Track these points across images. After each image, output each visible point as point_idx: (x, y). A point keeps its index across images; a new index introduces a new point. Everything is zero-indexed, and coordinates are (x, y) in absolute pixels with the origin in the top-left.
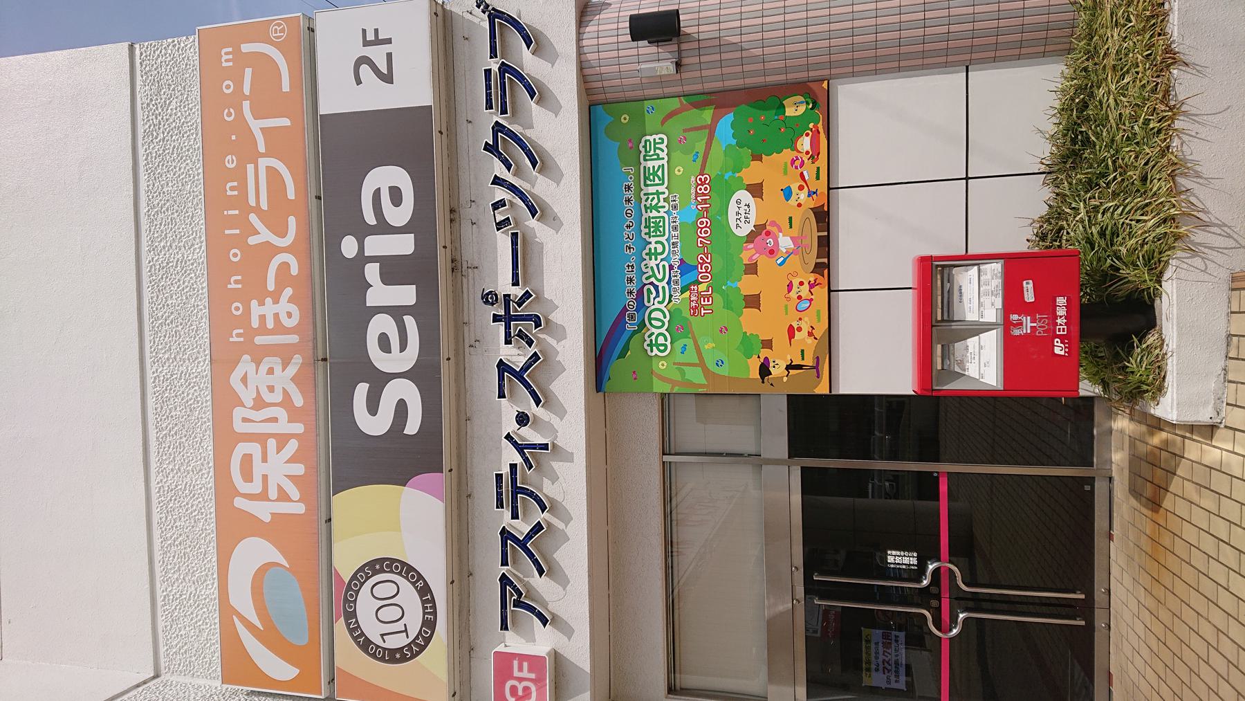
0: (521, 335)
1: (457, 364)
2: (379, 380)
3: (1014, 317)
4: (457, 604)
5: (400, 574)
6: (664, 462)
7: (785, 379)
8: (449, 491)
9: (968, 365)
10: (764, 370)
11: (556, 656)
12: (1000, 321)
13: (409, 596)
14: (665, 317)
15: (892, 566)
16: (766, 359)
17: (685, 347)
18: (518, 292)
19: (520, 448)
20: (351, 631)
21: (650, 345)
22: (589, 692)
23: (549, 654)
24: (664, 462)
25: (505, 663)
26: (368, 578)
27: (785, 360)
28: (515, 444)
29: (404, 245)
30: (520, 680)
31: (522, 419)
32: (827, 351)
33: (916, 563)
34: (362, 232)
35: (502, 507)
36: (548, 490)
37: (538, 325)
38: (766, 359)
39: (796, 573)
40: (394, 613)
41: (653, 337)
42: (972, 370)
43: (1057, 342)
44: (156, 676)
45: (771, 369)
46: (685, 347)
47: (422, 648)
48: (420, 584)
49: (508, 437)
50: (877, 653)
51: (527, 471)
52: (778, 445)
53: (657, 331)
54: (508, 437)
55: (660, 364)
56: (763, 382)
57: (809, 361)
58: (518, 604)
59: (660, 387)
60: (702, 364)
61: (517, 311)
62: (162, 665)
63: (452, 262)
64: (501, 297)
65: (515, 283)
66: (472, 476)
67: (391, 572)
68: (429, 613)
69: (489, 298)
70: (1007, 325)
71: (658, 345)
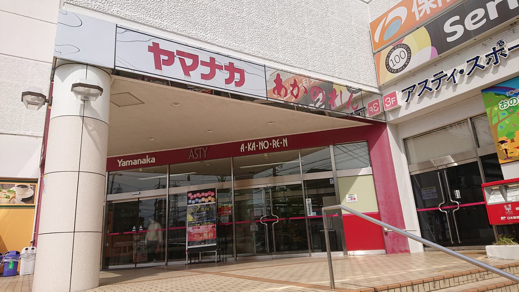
0: (490, 59)
1: (475, 43)
2: (461, 22)
3: (510, 205)
4: (405, 76)
5: (408, 57)
6: (467, 119)
7: (501, 149)
8: (436, 58)
9: (493, 196)
10: (503, 142)
11: (400, 107)
12: (508, 202)
13: (403, 62)
14: (514, 104)
15: (455, 192)
16: (507, 142)
17: (505, 114)
18: (507, 53)
19: (452, 75)
20: (390, 51)
21: (502, 102)
22: (394, 119)
23: (399, 105)
24: (467, 119)
25: (394, 95)
26: (404, 48)
27: (508, 147)
28: (453, 72)
30: (391, 101)
31: (462, 72)
32: (515, 160)
33: (458, 198)
35: (434, 77)
36: (443, 88)
37: (495, 64)
38: (507, 142)
39: (445, 166)
40: (398, 61)
41: (506, 103)
42: (492, 197)
43: (505, 217)
44: (367, 3)
45: (504, 144)
46: (505, 114)
47: (391, 72)
48: (406, 64)
49: (455, 69)
50: (430, 191)
51: (446, 80)
52: (482, 152)
53: (508, 103)
54: (455, 69)
55: (496, 108)
56: (498, 143)
57: (509, 155)
58: (409, 92)
59: (488, 110)
60: (500, 121)
61: (498, 54)
62: (370, 3)
63: (514, 23)
64: (503, 46)
65: (509, 50)
66: (442, 63)
67: (408, 54)
68: (400, 70)
69: (501, 43)
70: (507, 204)
71: (503, 105)
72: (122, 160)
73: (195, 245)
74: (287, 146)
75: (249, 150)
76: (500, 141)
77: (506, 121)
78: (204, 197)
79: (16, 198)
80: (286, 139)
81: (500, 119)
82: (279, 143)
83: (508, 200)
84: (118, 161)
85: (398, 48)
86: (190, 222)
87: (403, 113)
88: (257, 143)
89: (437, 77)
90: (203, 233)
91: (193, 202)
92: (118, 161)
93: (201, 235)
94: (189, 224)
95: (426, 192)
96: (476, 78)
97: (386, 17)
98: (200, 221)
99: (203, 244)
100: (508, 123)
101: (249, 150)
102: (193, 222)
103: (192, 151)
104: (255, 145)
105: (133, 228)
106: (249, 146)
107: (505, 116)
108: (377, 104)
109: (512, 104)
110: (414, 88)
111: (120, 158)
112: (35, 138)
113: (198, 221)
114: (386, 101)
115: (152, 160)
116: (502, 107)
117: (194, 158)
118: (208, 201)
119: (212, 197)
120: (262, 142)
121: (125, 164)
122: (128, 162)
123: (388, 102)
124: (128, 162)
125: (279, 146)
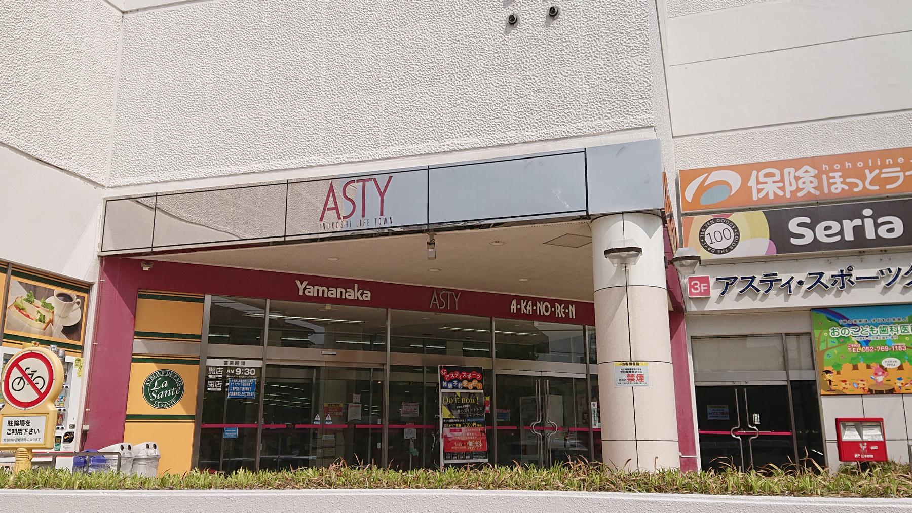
0: (836, 281)
2: (812, 227)
3: (866, 444)
5: (734, 239)
7: (825, 379)
10: (828, 372)
16: (832, 373)
19: (788, 282)
21: (834, 329)
28: (790, 280)
29: (870, 234)
30: (700, 286)
34: (874, 217)
38: (832, 373)
42: (847, 433)
43: (859, 455)
45: (829, 374)
48: (731, 247)
50: (720, 410)
53: (840, 332)
54: (792, 278)
57: (833, 388)
58: (727, 284)
60: (828, 349)
65: (857, 278)
70: (863, 442)
72: (305, 283)
73: (455, 459)
74: (574, 317)
75: (523, 313)
76: (825, 370)
77: (835, 351)
78: (466, 379)
79: (54, 323)
80: (574, 306)
81: (829, 347)
82: (564, 310)
83: (864, 438)
84: (298, 283)
85: (720, 222)
86: (446, 419)
87: (712, 306)
88: (534, 304)
89: (768, 278)
90: (468, 441)
91: (450, 386)
92: (298, 283)
93: (464, 443)
94: (444, 423)
95: (713, 410)
96: (814, 294)
97: (707, 174)
98: (464, 419)
99: (468, 459)
100: (836, 353)
101: (523, 313)
102: (450, 421)
103: (435, 294)
104: (531, 307)
105: (327, 419)
106: (523, 305)
107: (834, 345)
108: (692, 289)
109: (844, 334)
110: (735, 281)
111: (302, 278)
112: (91, 186)
113: (458, 419)
114: (692, 284)
115: (364, 296)
116: (833, 334)
117: (439, 308)
118: (472, 388)
119: (479, 381)
120: (541, 303)
121: (312, 292)
122: (318, 290)
123: (695, 286)
124: (318, 290)
125: (564, 316)
